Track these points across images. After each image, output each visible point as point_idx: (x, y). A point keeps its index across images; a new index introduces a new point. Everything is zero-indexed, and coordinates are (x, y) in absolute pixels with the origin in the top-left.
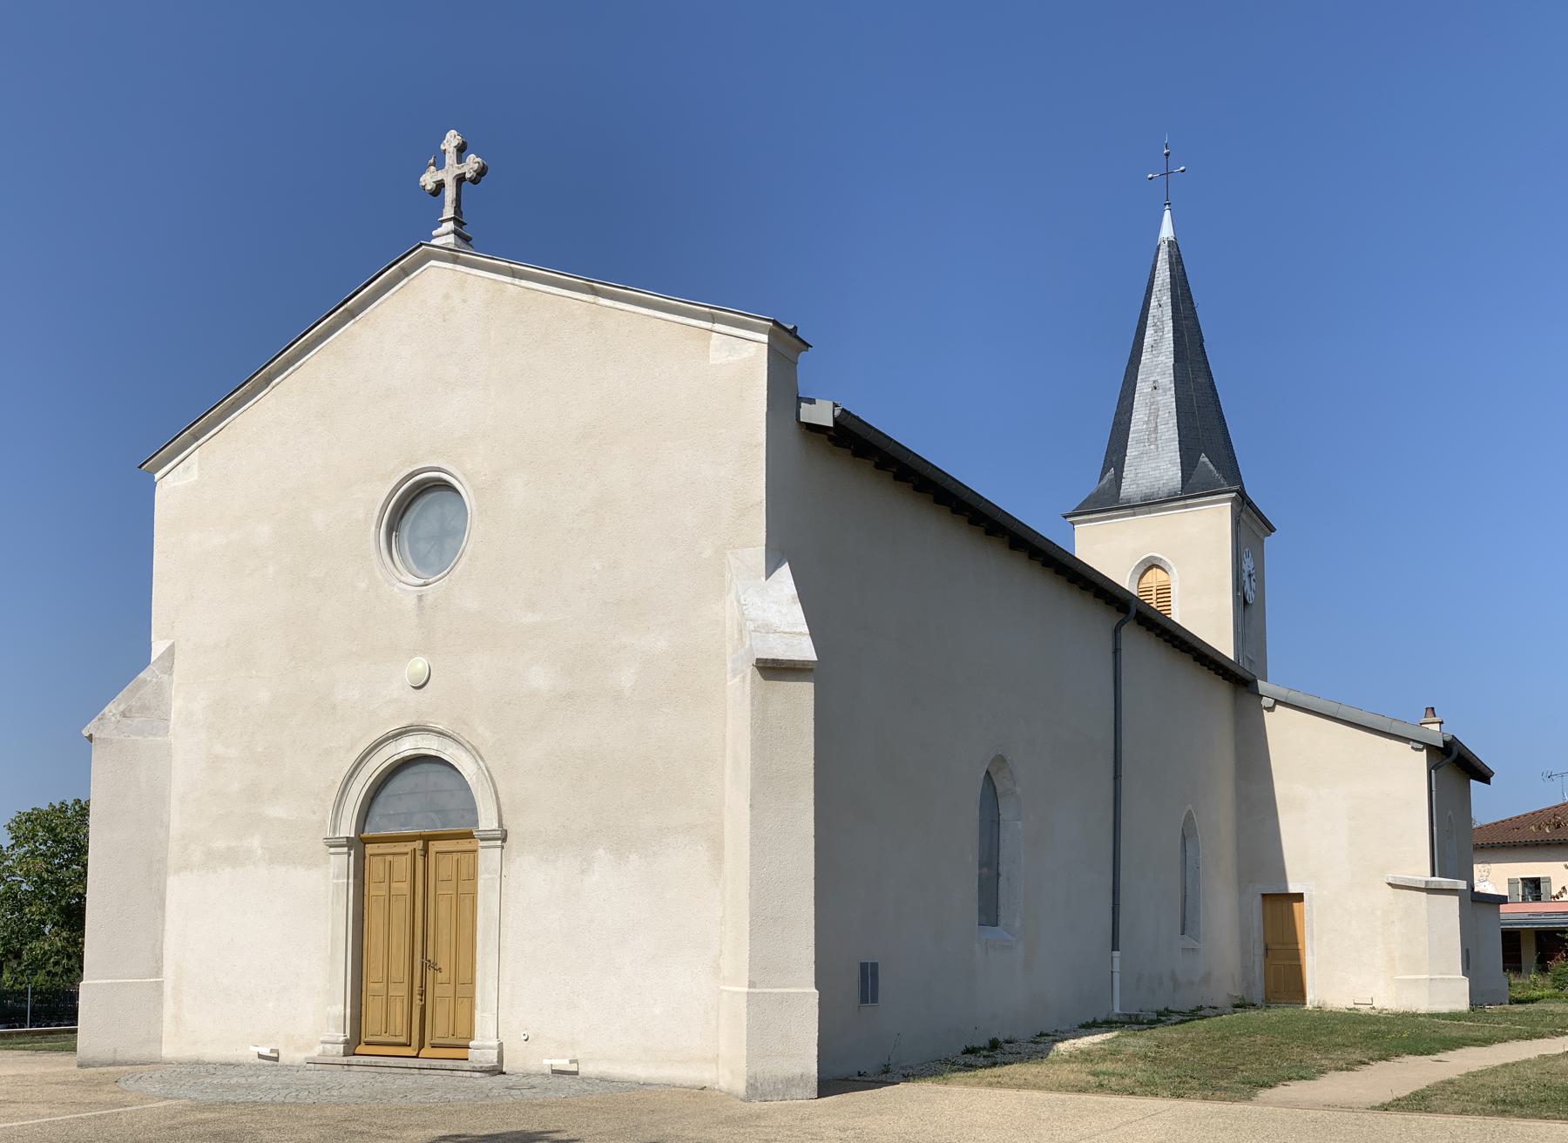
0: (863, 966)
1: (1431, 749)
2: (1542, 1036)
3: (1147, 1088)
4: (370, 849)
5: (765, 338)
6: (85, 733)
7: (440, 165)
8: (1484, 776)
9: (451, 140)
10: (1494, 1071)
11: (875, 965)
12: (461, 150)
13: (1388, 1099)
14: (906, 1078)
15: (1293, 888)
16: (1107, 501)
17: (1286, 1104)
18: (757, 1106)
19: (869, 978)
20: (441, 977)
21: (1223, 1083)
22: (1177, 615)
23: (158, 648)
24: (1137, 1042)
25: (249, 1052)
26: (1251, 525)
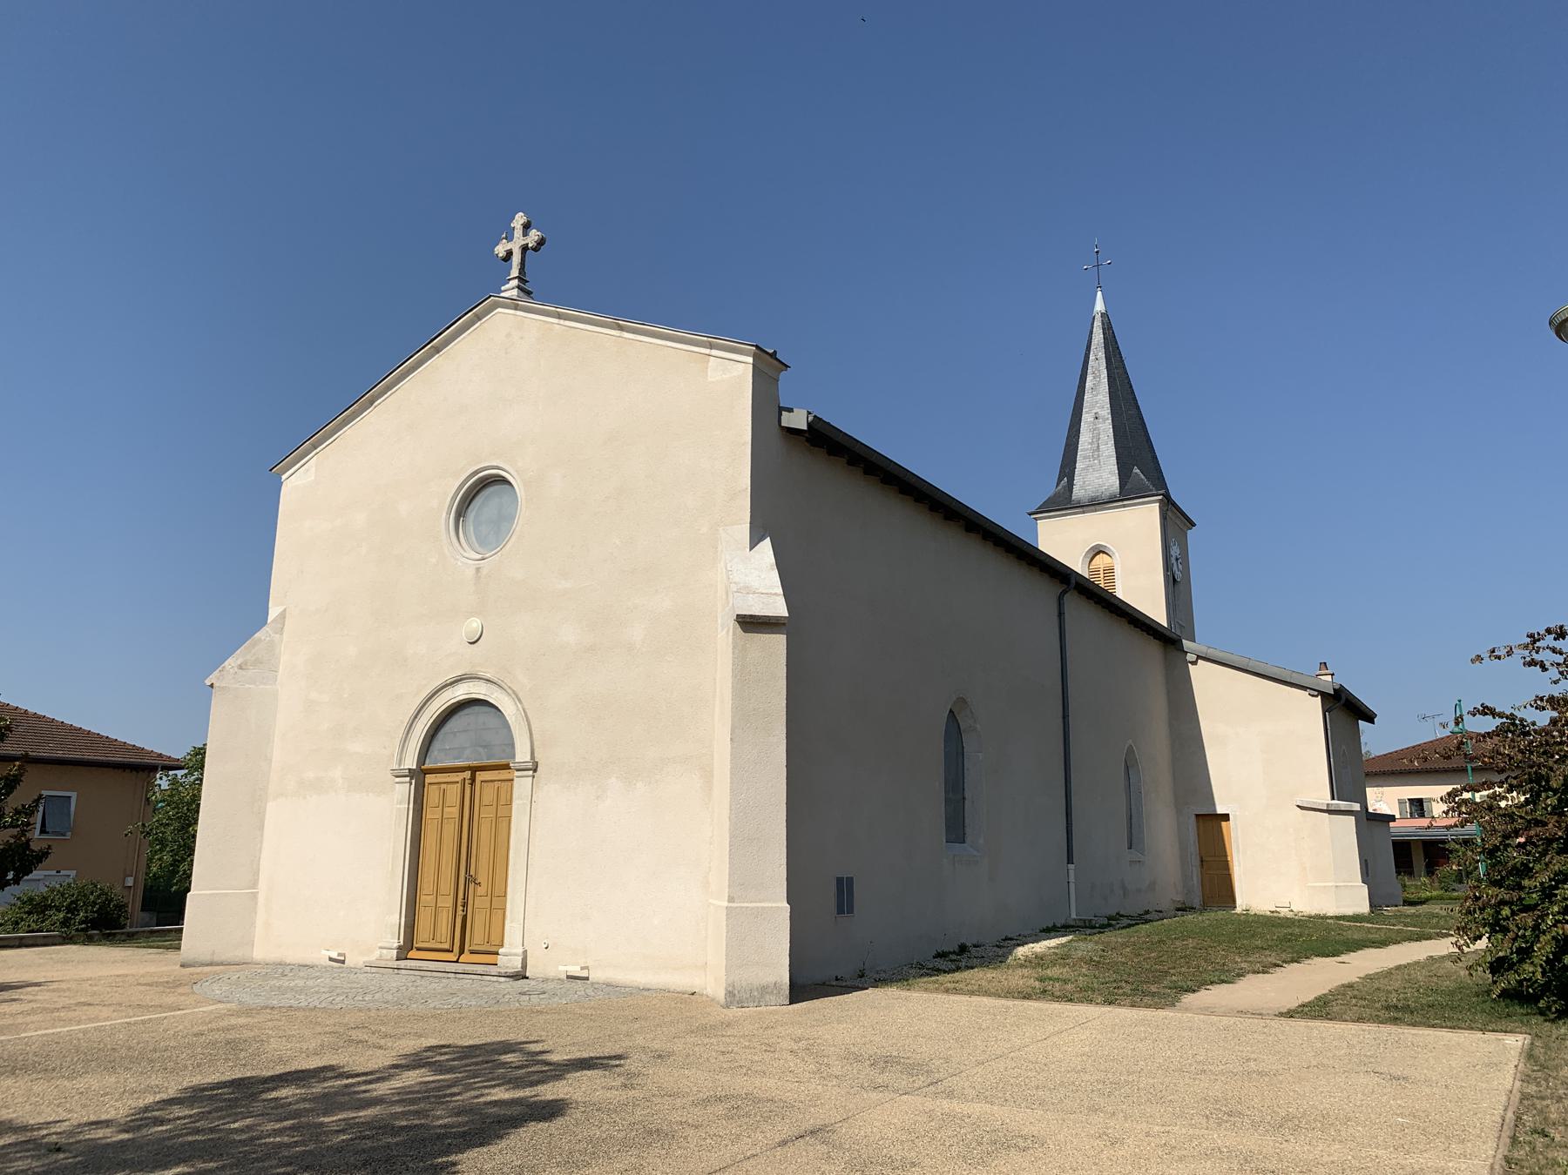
0: (840, 881)
1: (1323, 695)
2: (1429, 938)
3: (1084, 995)
4: (429, 778)
5: (750, 360)
6: (208, 683)
7: (510, 238)
8: (1370, 717)
9: (519, 220)
10: (1388, 974)
11: (850, 880)
12: (527, 227)
13: (1294, 1005)
14: (879, 982)
15: (1220, 810)
16: (1062, 502)
17: (1208, 1011)
18: (734, 1011)
19: (845, 892)
20: (481, 890)
21: (1153, 988)
22: (1120, 594)
23: (274, 612)
24: (1087, 946)
25: (322, 956)
26: (1175, 522)
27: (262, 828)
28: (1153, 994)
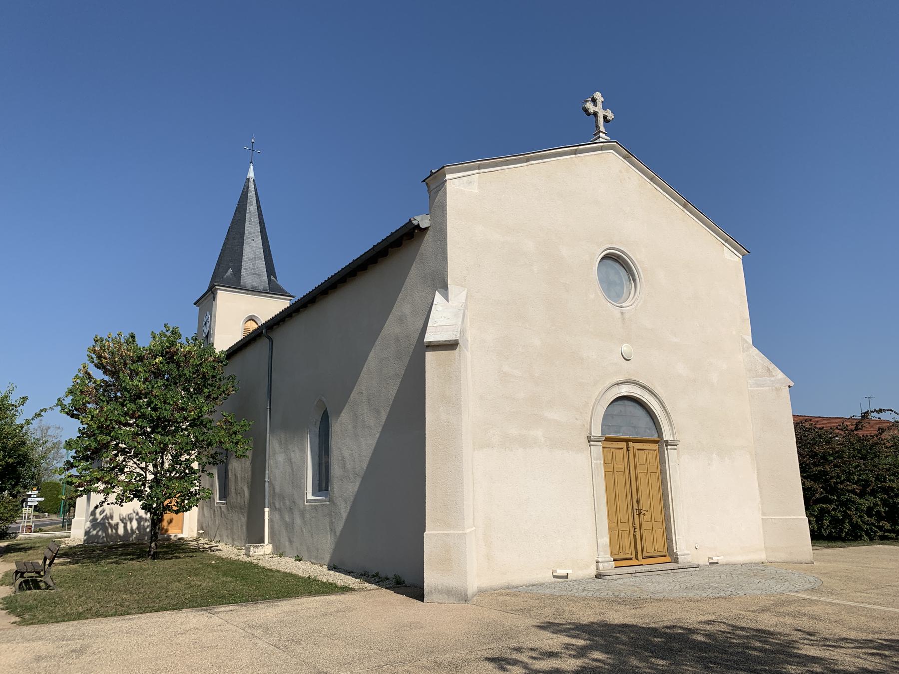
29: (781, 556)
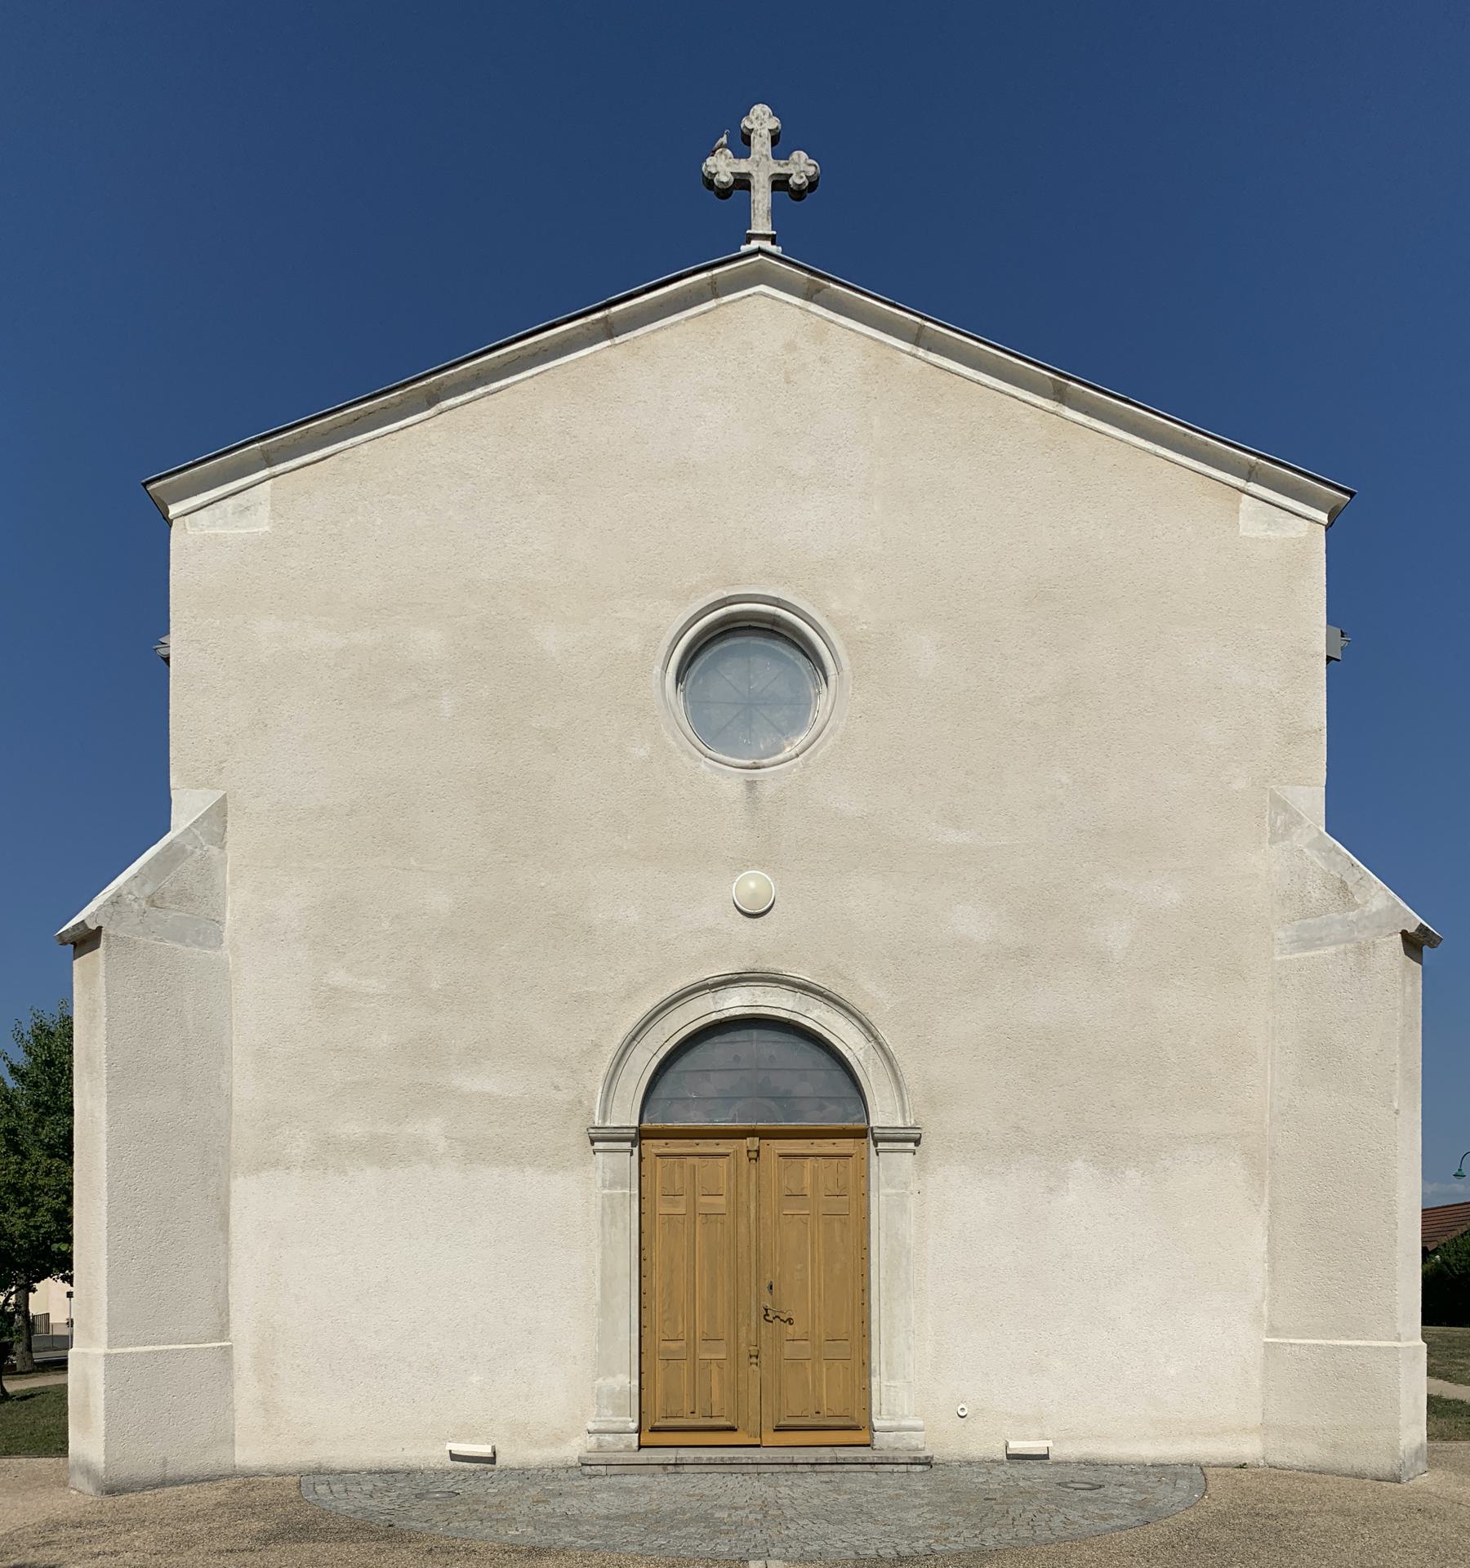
23: (187, 805)
27: (224, 1226)
28: (195, 1518)
29: (1305, 1452)
